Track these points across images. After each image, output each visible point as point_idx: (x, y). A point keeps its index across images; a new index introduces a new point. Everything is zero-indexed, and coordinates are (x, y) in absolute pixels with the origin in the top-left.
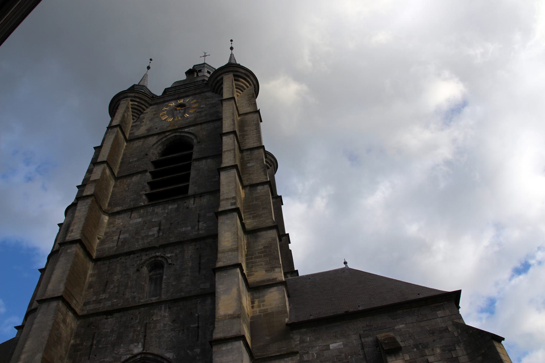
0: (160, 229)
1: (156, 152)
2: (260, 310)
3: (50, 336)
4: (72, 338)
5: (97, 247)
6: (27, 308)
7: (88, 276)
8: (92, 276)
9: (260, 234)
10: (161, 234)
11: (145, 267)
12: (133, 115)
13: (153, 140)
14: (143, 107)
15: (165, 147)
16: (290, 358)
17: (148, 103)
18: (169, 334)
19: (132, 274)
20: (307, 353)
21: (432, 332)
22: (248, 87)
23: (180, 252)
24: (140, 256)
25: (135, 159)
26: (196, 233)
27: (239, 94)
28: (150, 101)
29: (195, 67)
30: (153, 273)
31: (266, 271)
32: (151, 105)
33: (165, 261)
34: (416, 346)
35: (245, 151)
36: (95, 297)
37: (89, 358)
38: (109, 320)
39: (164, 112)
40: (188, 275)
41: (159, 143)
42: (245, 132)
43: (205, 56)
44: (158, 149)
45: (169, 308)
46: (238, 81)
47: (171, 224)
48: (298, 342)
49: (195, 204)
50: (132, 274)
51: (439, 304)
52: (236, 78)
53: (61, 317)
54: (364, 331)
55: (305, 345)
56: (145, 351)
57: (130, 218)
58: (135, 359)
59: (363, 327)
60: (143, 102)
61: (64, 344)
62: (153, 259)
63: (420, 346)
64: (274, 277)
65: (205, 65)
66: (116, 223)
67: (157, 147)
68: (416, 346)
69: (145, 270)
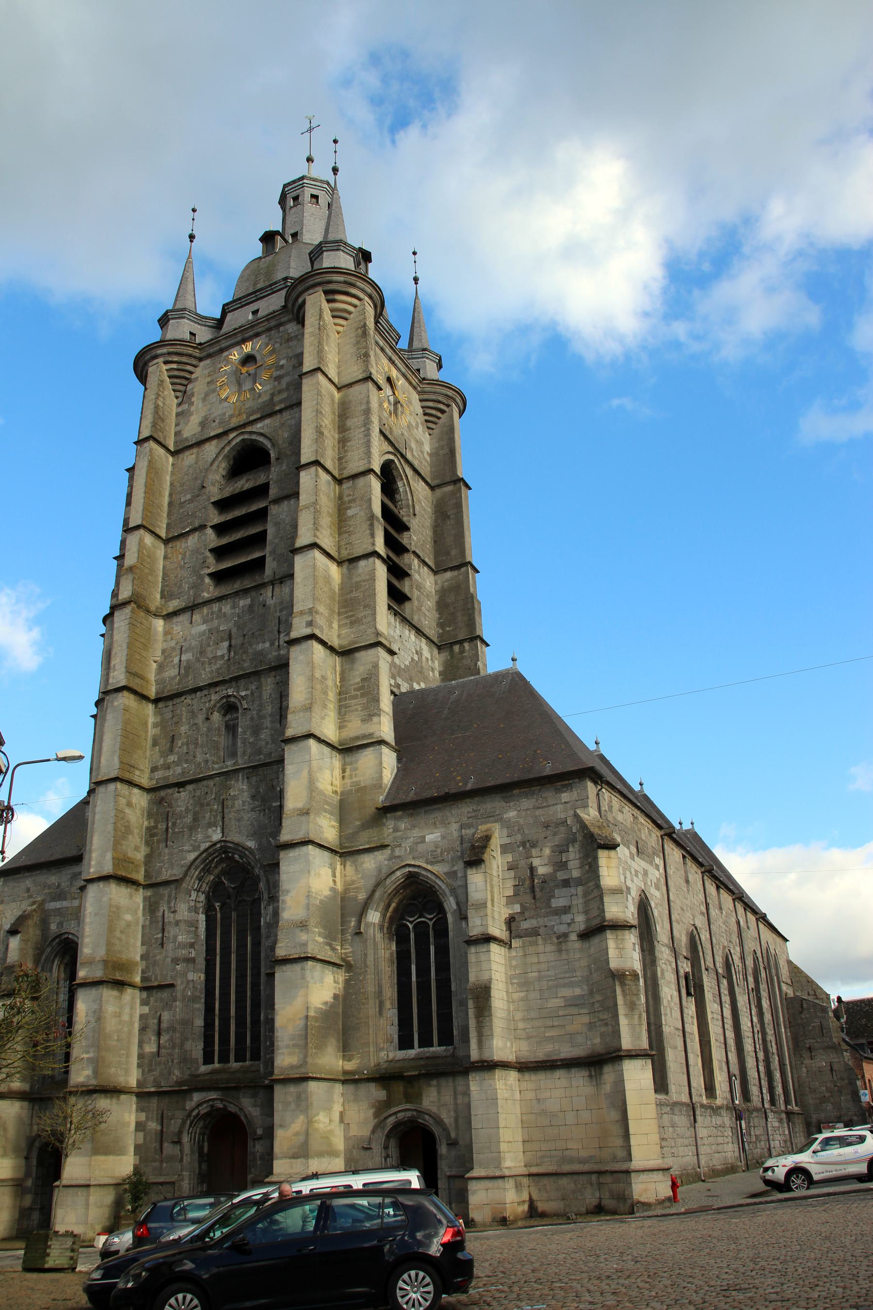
0: (230, 646)
1: (218, 477)
2: (351, 782)
3: (115, 830)
4: (145, 819)
7: (150, 725)
8: (155, 725)
9: (358, 655)
10: (232, 653)
11: (215, 713)
12: (174, 391)
13: (211, 450)
14: (189, 368)
15: (231, 463)
16: (380, 852)
17: (195, 357)
18: (249, 815)
19: (201, 724)
20: (400, 846)
22: (355, 306)
25: (189, 497)
26: (276, 653)
27: (340, 329)
28: (197, 353)
29: (286, 189)
30: (228, 717)
31: (363, 721)
32: (201, 360)
33: (239, 704)
34: (523, 844)
35: (345, 481)
36: (162, 759)
37: (167, 846)
38: (181, 794)
39: (223, 379)
40: (267, 728)
41: (220, 458)
42: (347, 433)
43: (310, 130)
44: (221, 469)
45: (247, 778)
46: (334, 301)
47: (244, 635)
48: (391, 830)
50: (201, 724)
51: (567, 782)
52: (330, 297)
53: (123, 801)
54: (468, 818)
55: (398, 834)
56: (224, 839)
57: (191, 623)
58: (215, 847)
59: (468, 812)
60: (184, 359)
61: (136, 831)
62: (224, 700)
63: (528, 844)
64: (371, 731)
65: (305, 181)
66: (174, 632)
67: (218, 467)
68: (523, 844)
69: (216, 716)
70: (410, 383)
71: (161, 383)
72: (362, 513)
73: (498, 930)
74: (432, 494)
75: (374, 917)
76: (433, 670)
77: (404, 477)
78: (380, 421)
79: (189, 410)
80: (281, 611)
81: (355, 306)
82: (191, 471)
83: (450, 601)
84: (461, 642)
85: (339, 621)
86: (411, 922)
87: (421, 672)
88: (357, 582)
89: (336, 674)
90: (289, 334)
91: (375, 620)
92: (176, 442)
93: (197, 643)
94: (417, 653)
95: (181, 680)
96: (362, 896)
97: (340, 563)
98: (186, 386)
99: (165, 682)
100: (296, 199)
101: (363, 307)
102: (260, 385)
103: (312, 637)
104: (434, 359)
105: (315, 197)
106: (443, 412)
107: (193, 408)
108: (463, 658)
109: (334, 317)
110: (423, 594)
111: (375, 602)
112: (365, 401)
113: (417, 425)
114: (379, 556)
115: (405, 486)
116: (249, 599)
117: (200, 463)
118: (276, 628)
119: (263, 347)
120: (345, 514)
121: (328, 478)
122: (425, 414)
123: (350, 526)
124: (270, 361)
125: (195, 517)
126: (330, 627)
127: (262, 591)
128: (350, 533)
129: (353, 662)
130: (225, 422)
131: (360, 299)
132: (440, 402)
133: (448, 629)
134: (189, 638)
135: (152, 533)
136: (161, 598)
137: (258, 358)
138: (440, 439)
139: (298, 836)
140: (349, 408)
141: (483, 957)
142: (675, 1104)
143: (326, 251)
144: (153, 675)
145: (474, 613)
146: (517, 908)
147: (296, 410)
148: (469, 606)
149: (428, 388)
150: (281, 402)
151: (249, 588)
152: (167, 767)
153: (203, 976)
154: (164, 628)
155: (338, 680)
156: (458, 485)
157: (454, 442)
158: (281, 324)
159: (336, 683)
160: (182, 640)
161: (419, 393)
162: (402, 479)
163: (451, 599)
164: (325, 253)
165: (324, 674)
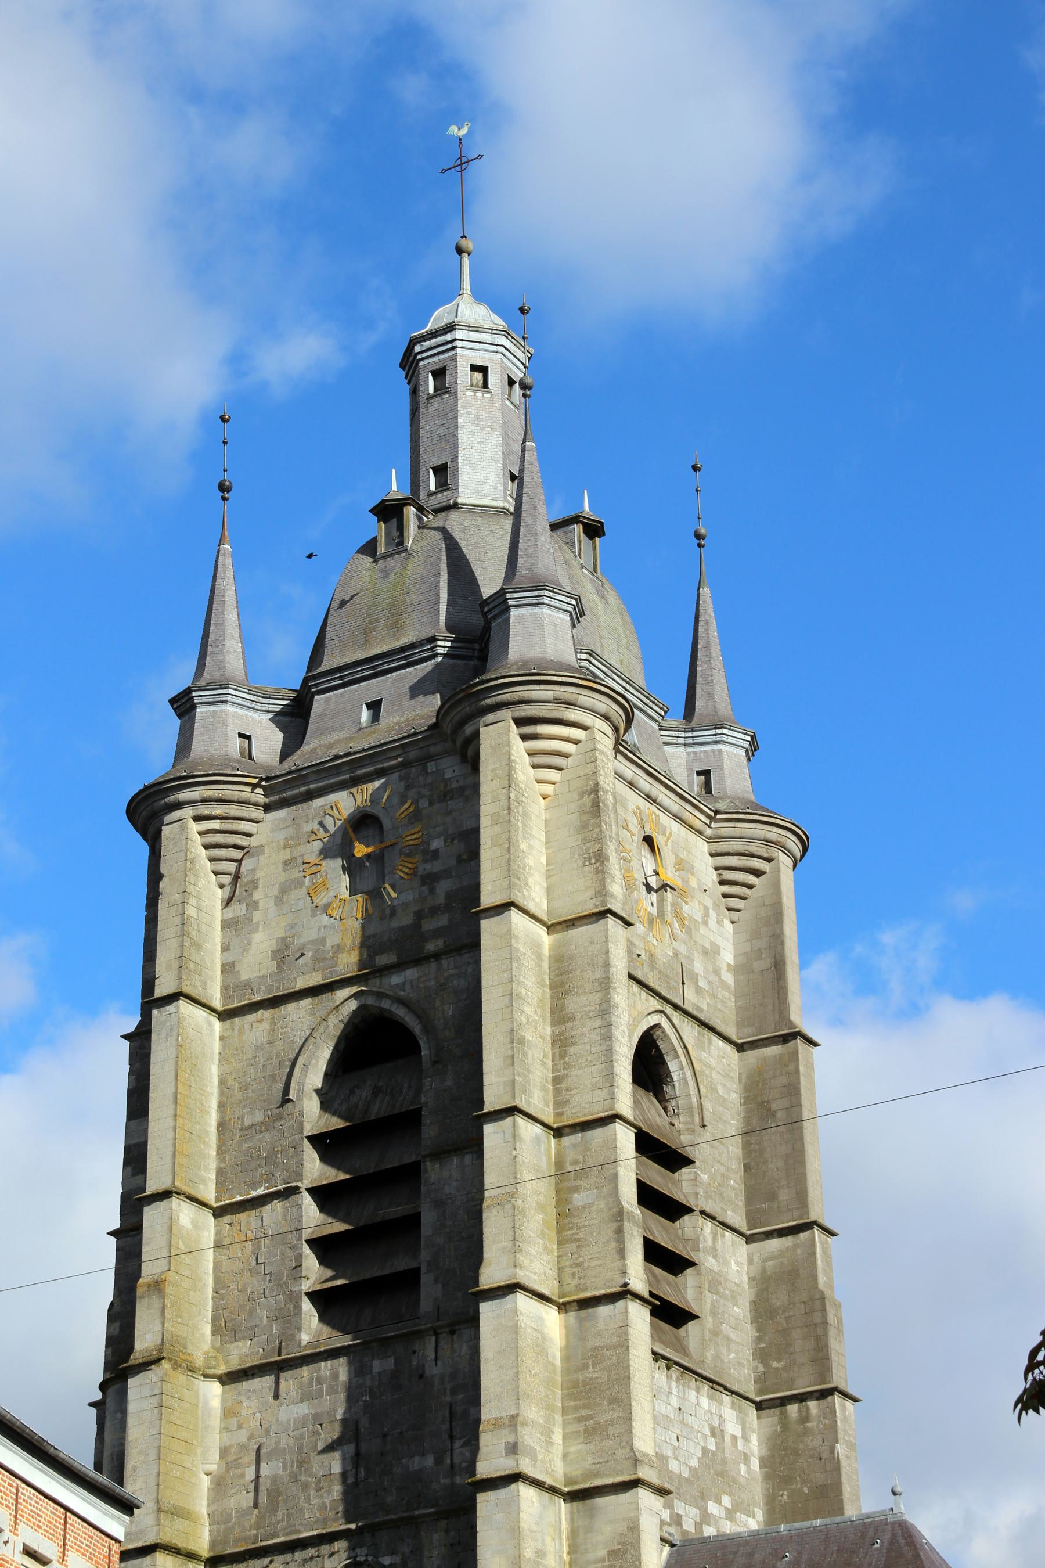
5: (208, 1505)
6: (115, 1252)
22: (576, 742)
23: (411, 1552)
24: (318, 1556)
27: (549, 789)
42: (568, 1025)
46: (535, 737)
47: (385, 1436)
49: (439, 1363)
52: (528, 730)
57: (276, 1396)
70: (691, 827)
72: (601, 1204)
74: (741, 1059)
76: (746, 1458)
77: (680, 1051)
78: (629, 951)
80: (454, 1392)
81: (576, 742)
82: (261, 1060)
83: (778, 1304)
84: (801, 1398)
85: (565, 1424)
87: (722, 1474)
88: (595, 1349)
89: (560, 1538)
90: (446, 782)
91: (630, 1431)
92: (225, 988)
93: (291, 1441)
94: (713, 1434)
95: (261, 1518)
97: (563, 1307)
98: (239, 862)
99: (228, 1521)
100: (439, 374)
101: (590, 745)
102: (393, 887)
103: (515, 1477)
104: (741, 743)
106: (758, 873)
108: (806, 1432)
109: (535, 767)
110: (723, 1296)
111: (629, 1394)
112: (600, 961)
113: (706, 914)
114: (636, 1296)
115: (682, 1068)
116: (391, 1360)
117: (279, 1045)
118: (446, 1427)
119: (395, 800)
120: (568, 1201)
121: (538, 1129)
123: (579, 1228)
124: (412, 836)
125: (276, 1164)
126: (549, 1443)
127: (417, 1346)
128: (580, 1244)
129: (592, 1514)
130: (324, 959)
131: (584, 728)
132: (752, 855)
133: (775, 1365)
134: (274, 1428)
135: (192, 1199)
136: (214, 1333)
137: (387, 823)
138: (755, 935)
140: (571, 972)
143: (515, 606)
144: (205, 1503)
145: (826, 1335)
147: (467, 957)
148: (817, 1318)
149: (727, 829)
150: (437, 933)
151: (391, 1338)
154: (223, 1400)
155: (565, 1549)
156: (791, 1044)
157: (782, 944)
158: (430, 758)
159: (561, 1557)
160: (261, 1432)
161: (710, 840)
162: (677, 1057)
163: (779, 1299)
165: (540, 1546)
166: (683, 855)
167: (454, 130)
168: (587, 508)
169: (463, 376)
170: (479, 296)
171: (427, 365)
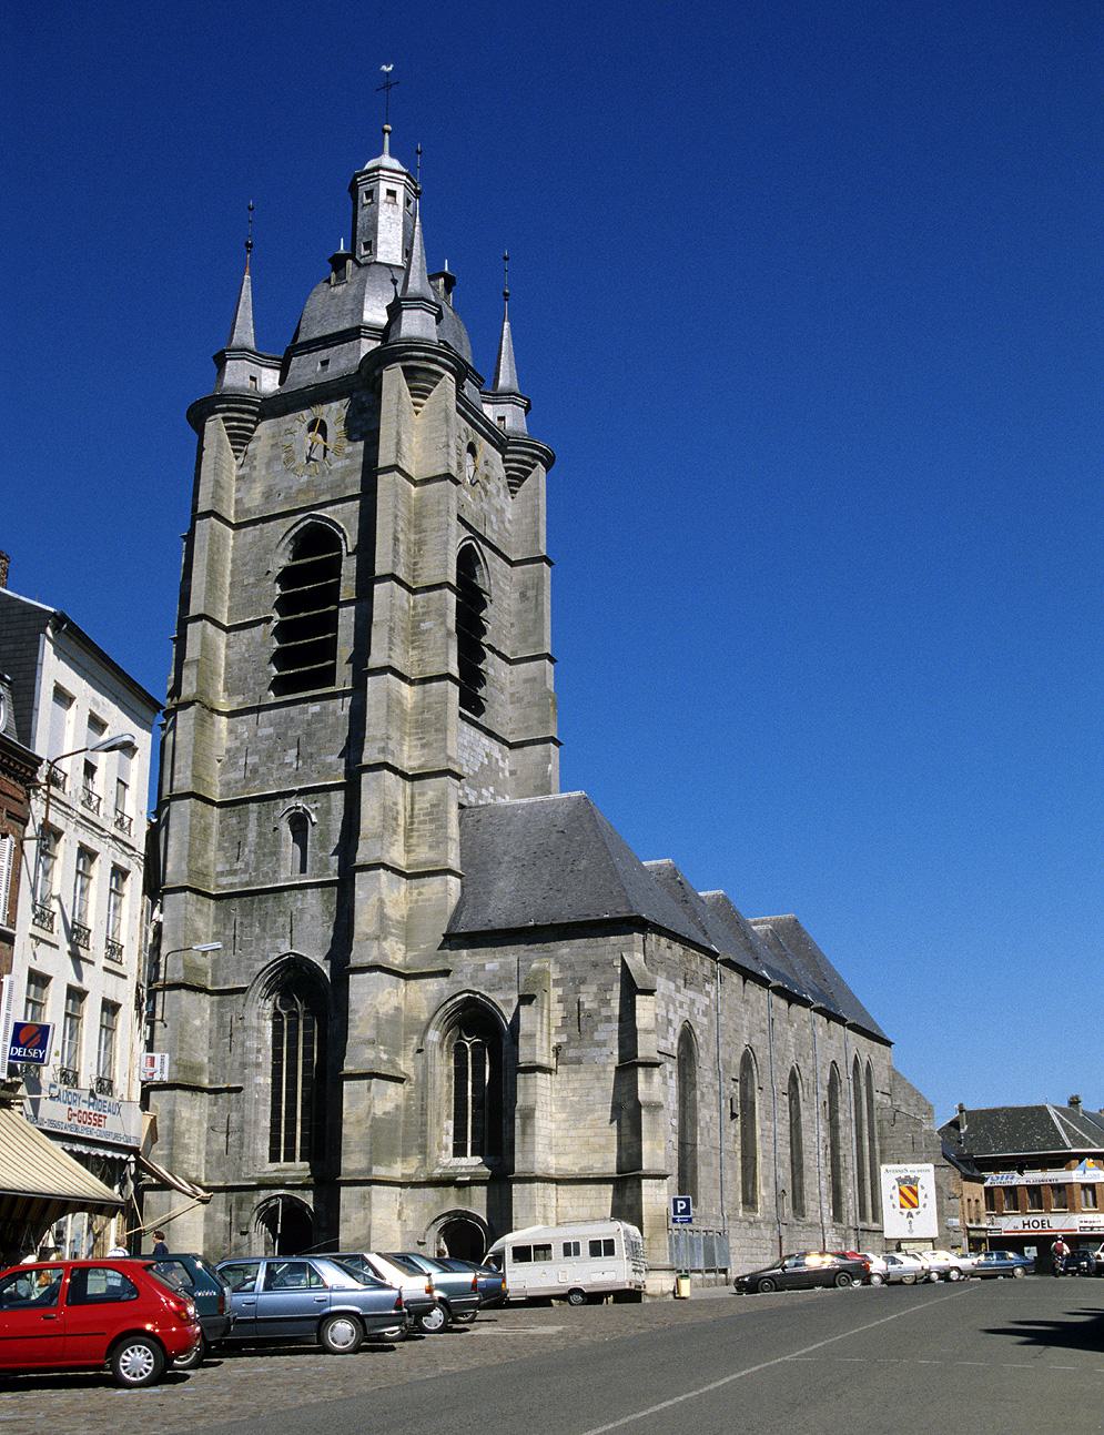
10: (300, 762)
21: (595, 965)
25: (252, 580)
31: (430, 847)
34: (573, 980)
41: (286, 540)
46: (415, 379)
68: (573, 980)
71: (220, 441)
73: (544, 1057)
75: (434, 1036)
76: (503, 770)
79: (250, 475)
86: (469, 1042)
90: (363, 403)
96: (424, 1017)
100: (369, 194)
105: (391, 193)
107: (255, 474)
113: (498, 491)
120: (418, 627)
122: (508, 476)
139: (369, 959)
141: (530, 1082)
142: (811, 1225)
146: (564, 1038)
152: (233, 872)
153: (269, 1081)
164: (404, 312)
166: (488, 457)
167: (384, 68)
168: (446, 269)
169: (383, 195)
170: (392, 155)
171: (362, 190)
